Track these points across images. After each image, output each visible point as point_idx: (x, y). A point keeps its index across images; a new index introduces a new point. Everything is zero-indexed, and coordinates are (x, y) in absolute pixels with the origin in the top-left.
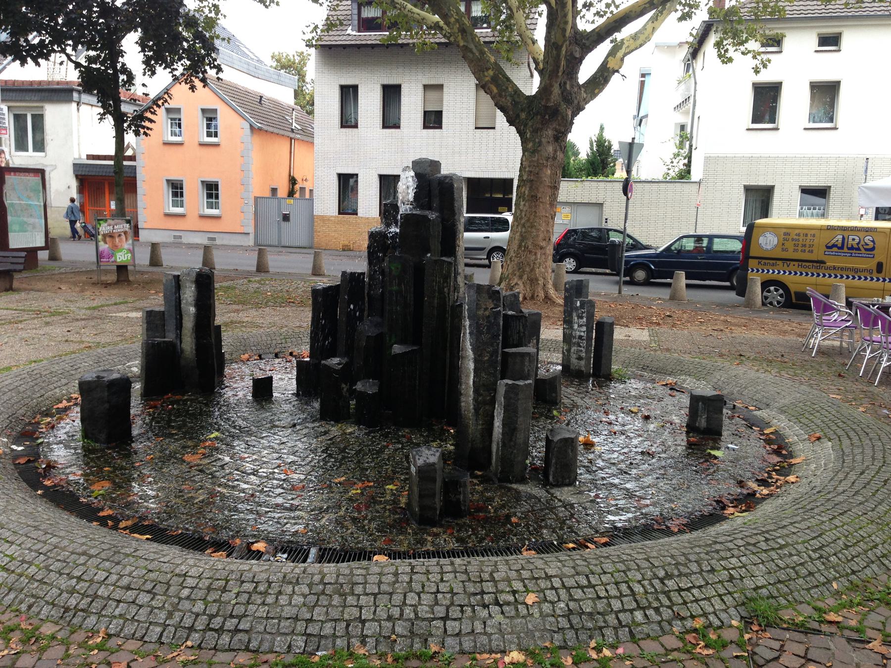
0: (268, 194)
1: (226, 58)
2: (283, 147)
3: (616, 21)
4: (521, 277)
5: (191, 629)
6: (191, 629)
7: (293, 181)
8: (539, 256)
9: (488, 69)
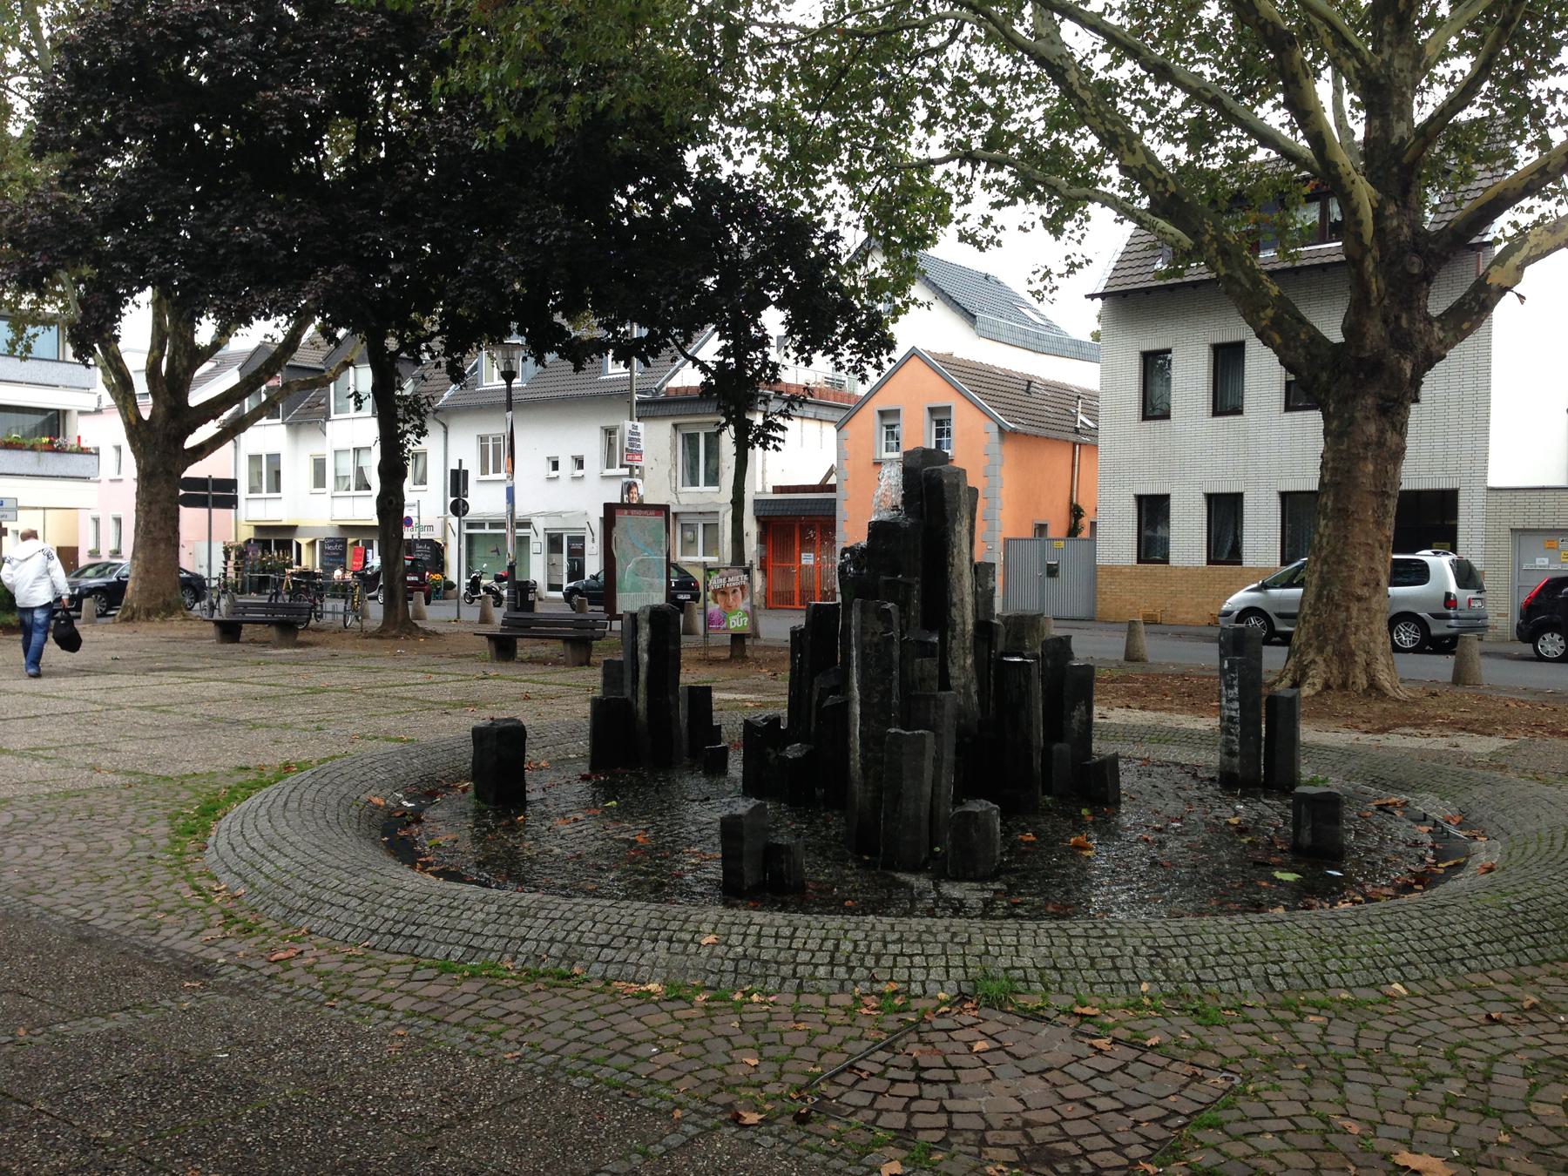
0: (1028, 532)
1: (987, 327)
2: (1059, 460)
3: (1481, 208)
4: (1320, 650)
5: (375, 931)
6: (375, 931)
7: (1076, 512)
8: (1354, 613)
9: (1264, 308)
